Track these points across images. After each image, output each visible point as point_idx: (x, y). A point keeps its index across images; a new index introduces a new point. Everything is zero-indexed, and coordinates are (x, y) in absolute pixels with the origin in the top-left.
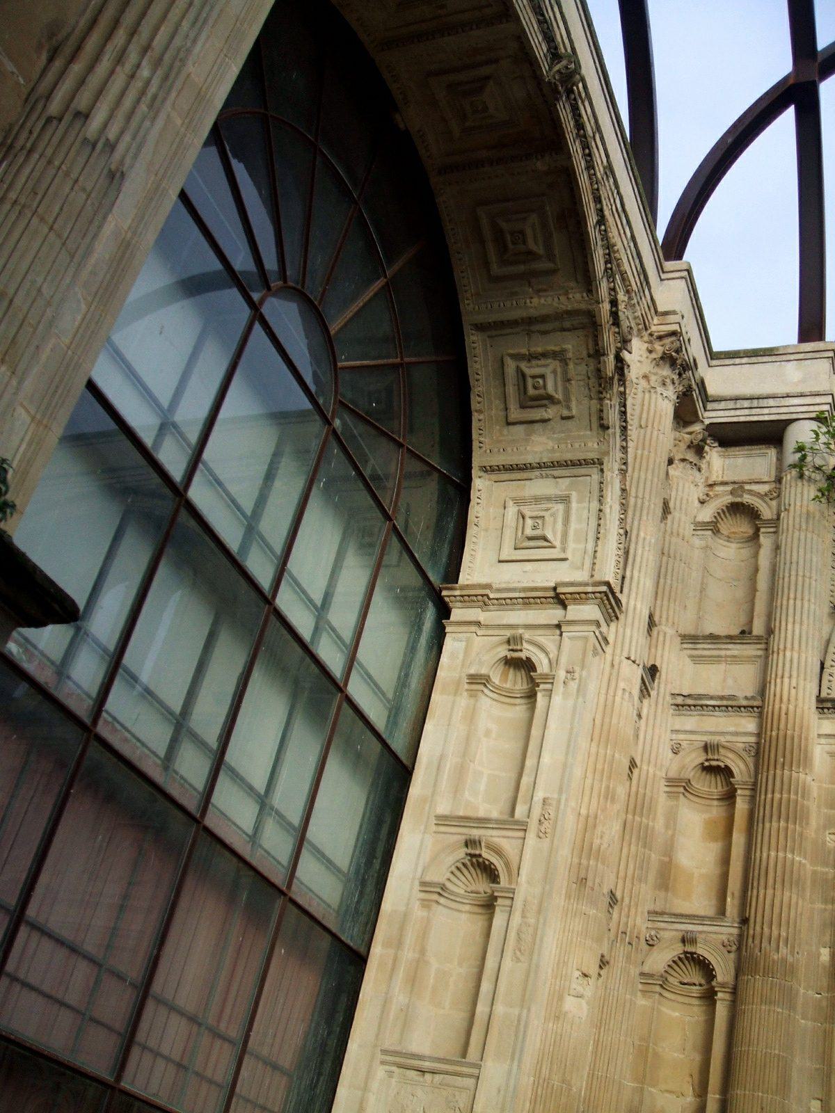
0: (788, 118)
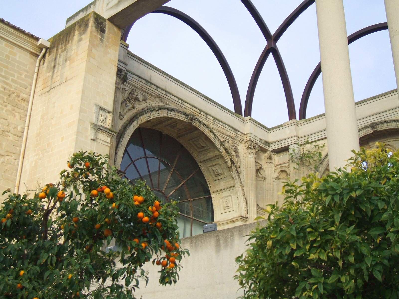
0: (271, 57)
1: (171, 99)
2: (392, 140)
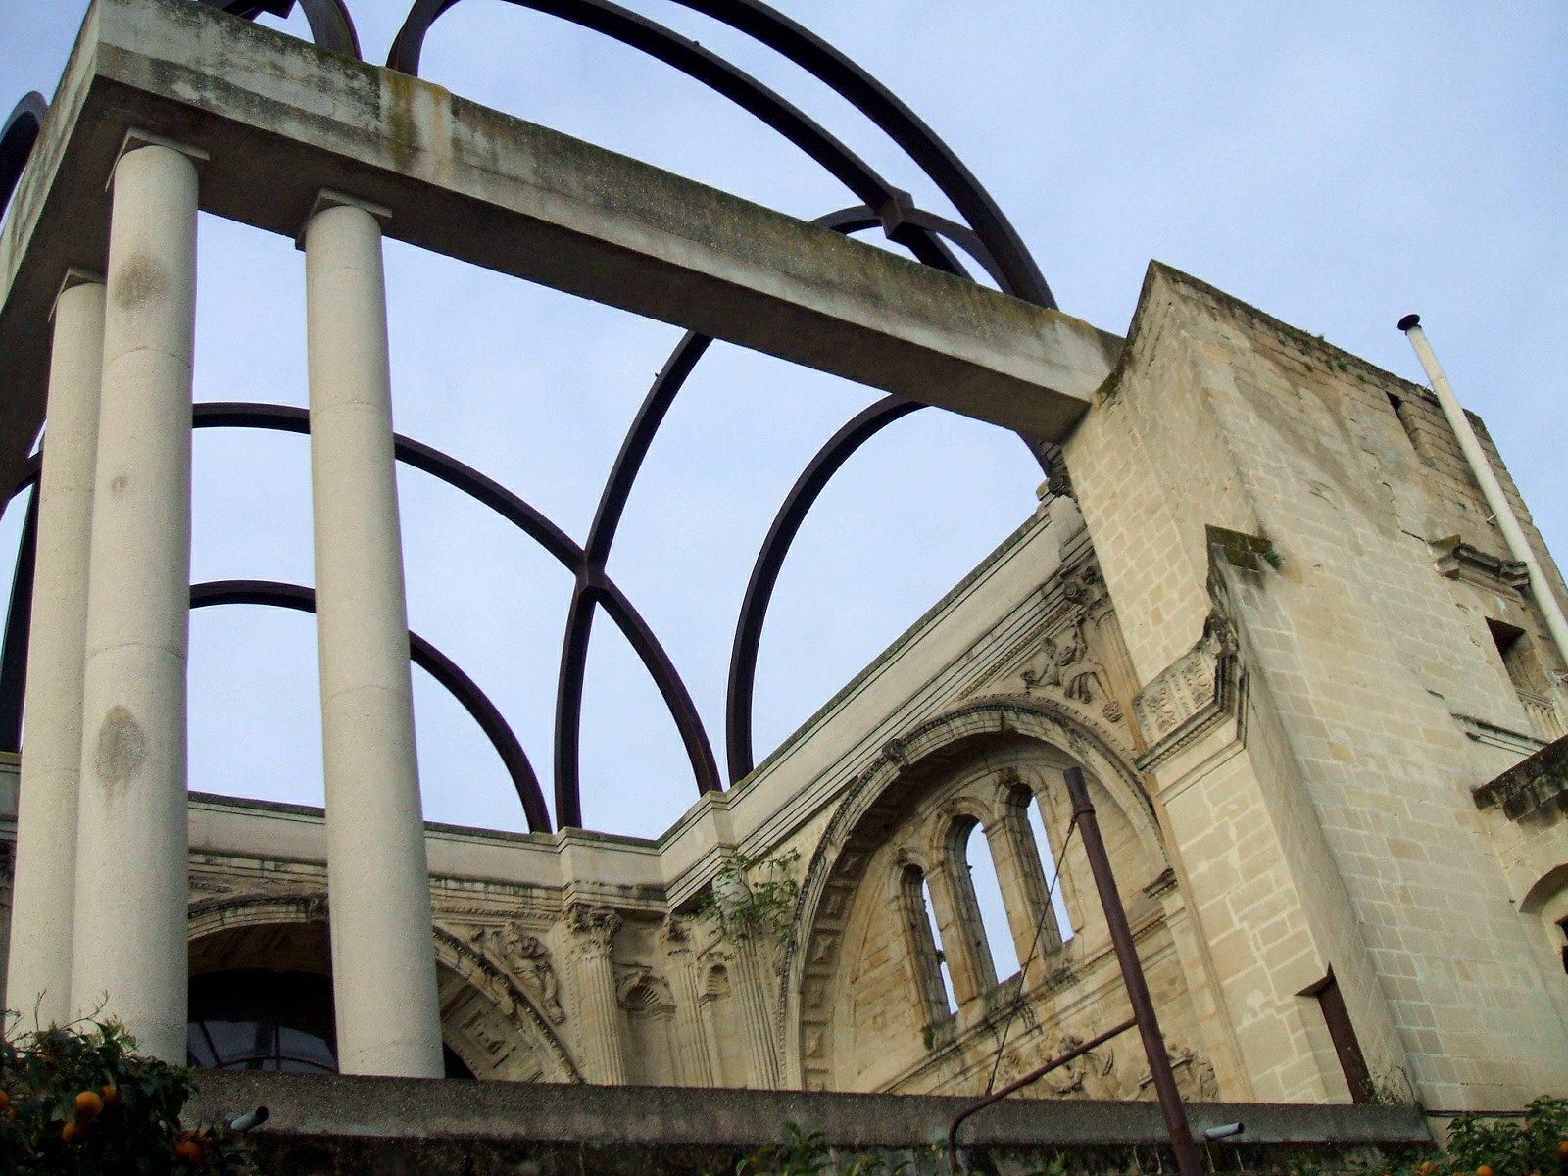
0: (600, 615)
1: (233, 871)
2: (971, 779)
